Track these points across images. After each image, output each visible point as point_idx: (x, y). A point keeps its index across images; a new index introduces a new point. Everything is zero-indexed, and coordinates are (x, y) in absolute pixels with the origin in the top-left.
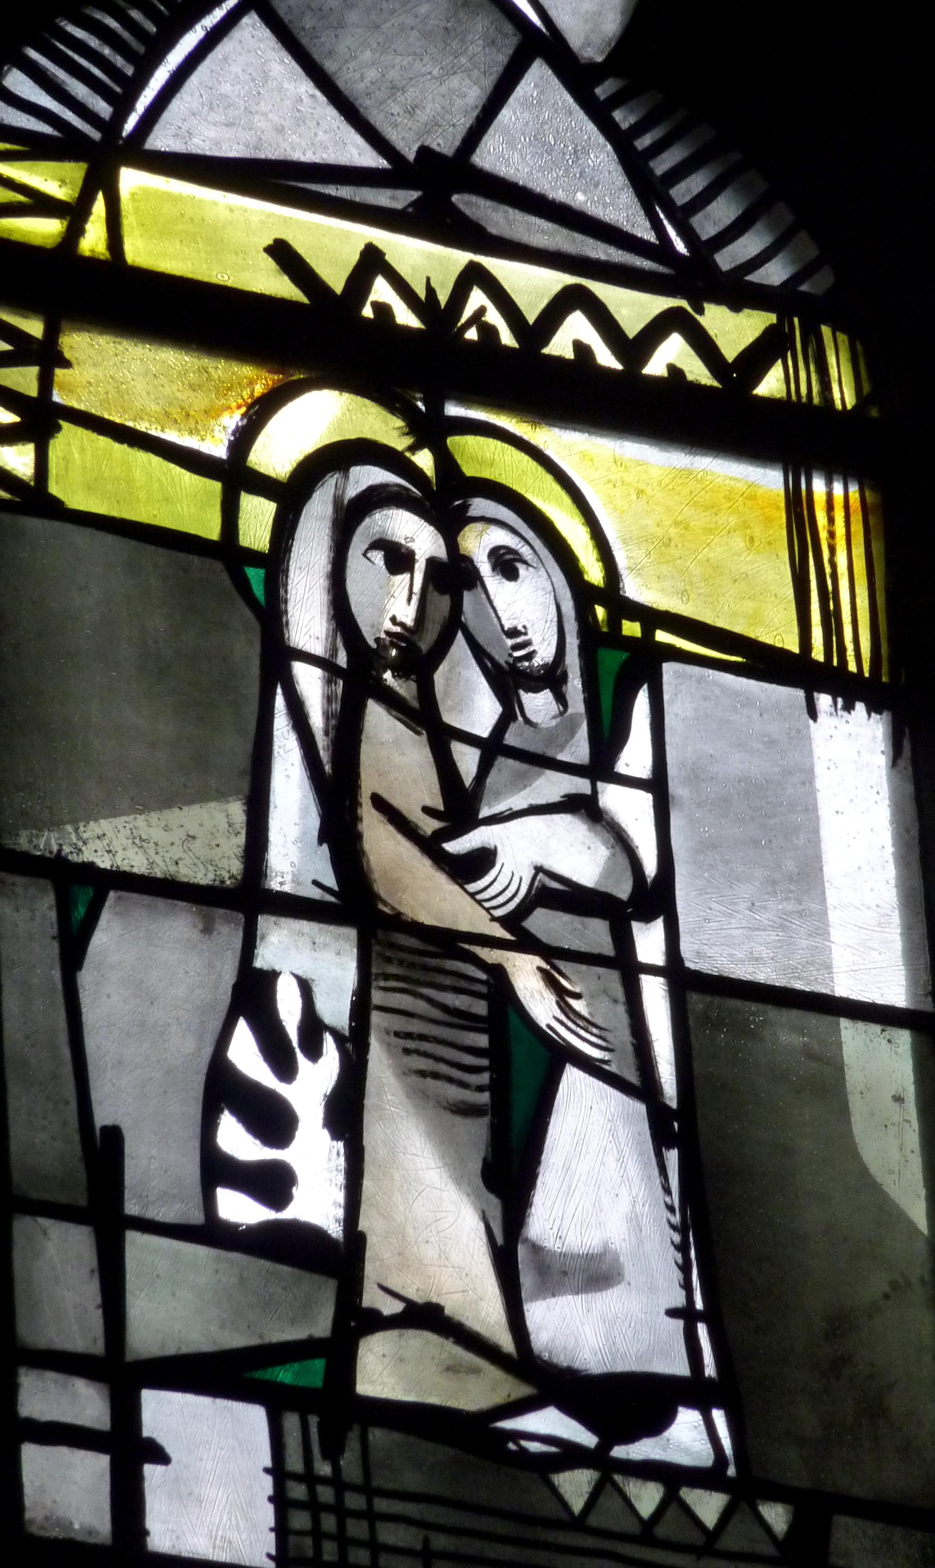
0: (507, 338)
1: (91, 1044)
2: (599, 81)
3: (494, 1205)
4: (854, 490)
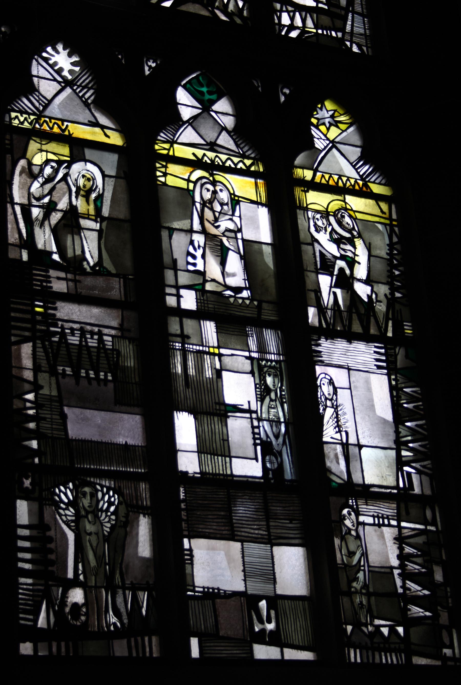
0: (221, 164)
1: (173, 248)
2: (231, 133)
3: (221, 267)
4: (263, 181)
